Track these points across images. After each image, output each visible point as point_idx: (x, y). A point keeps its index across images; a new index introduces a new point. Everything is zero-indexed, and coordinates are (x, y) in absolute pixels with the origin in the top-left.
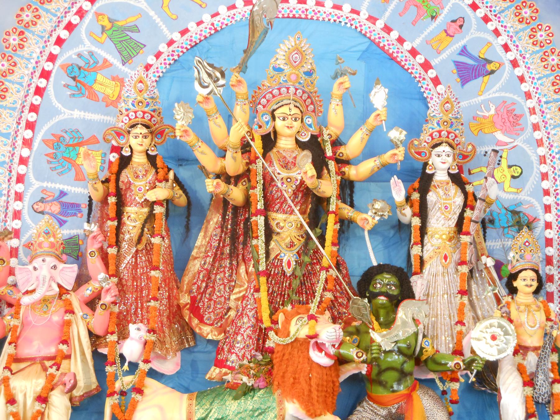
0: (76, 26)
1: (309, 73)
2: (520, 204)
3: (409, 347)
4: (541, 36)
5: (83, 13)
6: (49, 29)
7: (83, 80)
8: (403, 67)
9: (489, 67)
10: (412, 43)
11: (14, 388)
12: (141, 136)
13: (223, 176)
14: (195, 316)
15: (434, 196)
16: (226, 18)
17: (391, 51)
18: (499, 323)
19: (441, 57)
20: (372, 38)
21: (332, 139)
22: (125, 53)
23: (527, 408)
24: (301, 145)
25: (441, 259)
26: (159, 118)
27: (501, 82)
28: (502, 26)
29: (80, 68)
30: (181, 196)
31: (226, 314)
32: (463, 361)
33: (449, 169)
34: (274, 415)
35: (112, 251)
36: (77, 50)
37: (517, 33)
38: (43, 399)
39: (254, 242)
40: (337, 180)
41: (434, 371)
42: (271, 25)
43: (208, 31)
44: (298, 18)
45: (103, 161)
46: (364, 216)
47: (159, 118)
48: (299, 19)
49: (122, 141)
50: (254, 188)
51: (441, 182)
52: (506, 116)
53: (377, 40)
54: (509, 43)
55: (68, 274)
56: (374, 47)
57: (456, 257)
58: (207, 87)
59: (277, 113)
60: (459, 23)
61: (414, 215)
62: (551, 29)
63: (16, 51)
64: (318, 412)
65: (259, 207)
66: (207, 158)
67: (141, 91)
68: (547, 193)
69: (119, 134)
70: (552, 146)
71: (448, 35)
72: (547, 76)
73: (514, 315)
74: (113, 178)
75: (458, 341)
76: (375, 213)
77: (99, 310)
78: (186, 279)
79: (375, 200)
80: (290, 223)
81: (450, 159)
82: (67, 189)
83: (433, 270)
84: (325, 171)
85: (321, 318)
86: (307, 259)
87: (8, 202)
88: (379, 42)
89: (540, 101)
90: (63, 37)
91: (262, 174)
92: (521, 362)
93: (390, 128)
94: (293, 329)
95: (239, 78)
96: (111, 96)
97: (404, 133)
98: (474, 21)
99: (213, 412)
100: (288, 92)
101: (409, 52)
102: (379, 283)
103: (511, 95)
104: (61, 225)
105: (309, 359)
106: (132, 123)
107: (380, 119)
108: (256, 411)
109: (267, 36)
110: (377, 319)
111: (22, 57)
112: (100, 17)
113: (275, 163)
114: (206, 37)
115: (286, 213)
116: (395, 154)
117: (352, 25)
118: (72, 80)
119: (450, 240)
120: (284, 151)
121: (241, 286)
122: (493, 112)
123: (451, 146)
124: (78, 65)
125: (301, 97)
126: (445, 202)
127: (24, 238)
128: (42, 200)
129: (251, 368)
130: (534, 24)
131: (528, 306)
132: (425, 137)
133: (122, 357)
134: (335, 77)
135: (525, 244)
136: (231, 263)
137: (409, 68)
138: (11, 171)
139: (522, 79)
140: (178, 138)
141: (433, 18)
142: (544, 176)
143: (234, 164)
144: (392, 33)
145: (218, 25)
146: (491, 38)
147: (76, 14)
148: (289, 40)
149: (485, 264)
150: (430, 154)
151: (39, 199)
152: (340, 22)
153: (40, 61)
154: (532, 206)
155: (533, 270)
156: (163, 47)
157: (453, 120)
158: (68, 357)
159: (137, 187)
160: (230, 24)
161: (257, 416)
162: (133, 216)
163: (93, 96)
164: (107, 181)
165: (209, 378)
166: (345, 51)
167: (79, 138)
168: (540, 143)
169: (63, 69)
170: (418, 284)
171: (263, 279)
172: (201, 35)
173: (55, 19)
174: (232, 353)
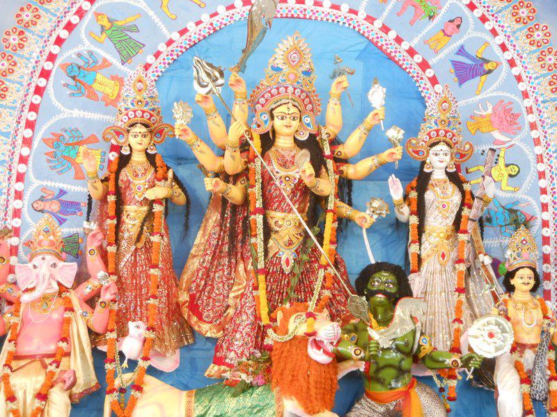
0: (75, 25)
12: (140, 135)
15: (432, 194)
17: (389, 51)
22: (124, 53)
24: (299, 144)
25: (438, 258)
26: (158, 118)
29: (79, 67)
33: (446, 167)
36: (76, 50)
39: (253, 240)
43: (207, 30)
46: (362, 214)
47: (158, 118)
49: (121, 140)
50: (253, 186)
58: (206, 86)
59: (275, 112)
60: (456, 23)
61: (412, 213)
65: (257, 206)
66: (206, 157)
67: (140, 91)
69: (118, 133)
71: (445, 34)
76: (373, 212)
80: (289, 221)
81: (448, 158)
84: (324, 170)
95: (238, 77)
96: (111, 95)
98: (471, 21)
100: (286, 92)
112: (100, 17)
114: (205, 37)
116: (393, 153)
117: (350, 25)
119: (448, 238)
123: (448, 145)
124: (77, 65)
125: (300, 96)
132: (423, 136)
134: (334, 77)
140: (177, 137)
143: (232, 163)
148: (287, 40)
150: (428, 153)
152: (338, 22)
156: (162, 47)
162: (132, 215)
163: (92, 95)
164: (106, 180)
172: (199, 35)
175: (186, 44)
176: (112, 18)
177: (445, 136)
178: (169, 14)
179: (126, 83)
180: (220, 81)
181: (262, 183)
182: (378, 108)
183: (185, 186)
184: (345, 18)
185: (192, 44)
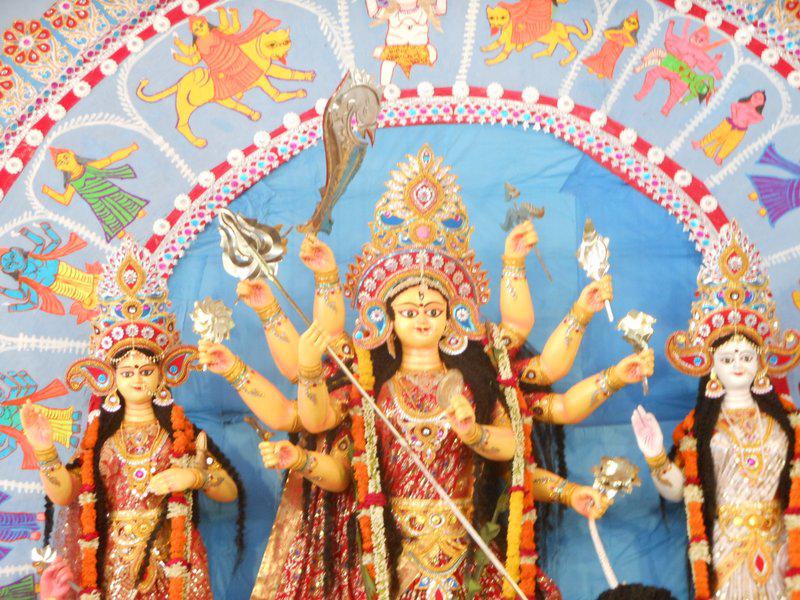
0: (16, 176)
1: (454, 223)
5: (28, 153)
7: (32, 277)
8: (650, 196)
10: (664, 149)
12: (136, 371)
15: (725, 441)
16: (300, 136)
17: (624, 169)
20: (585, 147)
21: (512, 346)
22: (110, 219)
24: (448, 361)
25: (750, 567)
26: (171, 335)
29: (26, 255)
30: (221, 480)
33: (752, 385)
36: (19, 222)
39: (366, 559)
42: (371, 138)
43: (266, 162)
44: (438, 123)
45: (75, 428)
46: (584, 491)
47: (171, 335)
48: (439, 126)
49: (102, 384)
50: (359, 453)
51: (738, 413)
53: (595, 151)
56: (591, 164)
58: (247, 264)
59: (396, 305)
60: (754, 103)
61: (688, 481)
62: (4, 47)
65: (371, 490)
66: (261, 399)
67: (131, 286)
69: (96, 372)
71: (734, 127)
76: (607, 484)
79: (606, 458)
80: (435, 517)
81: (752, 366)
82: (9, 488)
84: (501, 409)
88: (600, 154)
91: (373, 424)
95: (318, 243)
96: (87, 302)
97: (650, 320)
98: (784, 95)
100: (414, 262)
107: (598, 300)
112: (61, 157)
113: (397, 400)
114: (263, 176)
115: (427, 497)
116: (635, 365)
117: (542, 126)
118: (10, 278)
119: (766, 527)
120: (415, 376)
123: (751, 339)
124: (21, 250)
125: (442, 269)
132: (697, 326)
134: (508, 226)
137: (661, 199)
140: (205, 368)
141: (702, 97)
143: (315, 409)
145: (284, 151)
147: (14, 155)
148: (408, 163)
150: (712, 360)
152: (520, 123)
156: (182, 202)
157: (749, 289)
159: (134, 469)
160: (307, 147)
162: (128, 528)
163: (52, 305)
164: (76, 465)
166: (535, 176)
167: (29, 387)
172: (253, 172)
175: (227, 192)
176: (85, 154)
177: (742, 322)
178: (191, 138)
179: (103, 279)
180: (275, 251)
181: (379, 445)
182: (596, 276)
183: (233, 463)
184: (533, 113)
185: (240, 190)
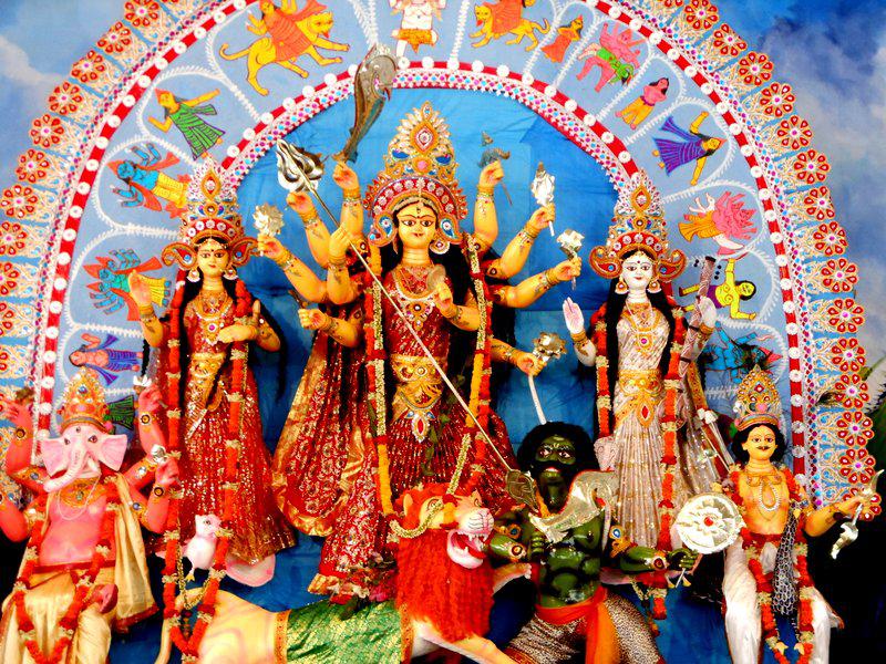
0: (129, 109)
1: (445, 159)
2: (754, 335)
3: (590, 539)
4: (777, 100)
6: (93, 115)
7: (139, 183)
9: (705, 146)
11: (31, 608)
12: (212, 254)
13: (327, 306)
14: (294, 505)
15: (627, 326)
16: (336, 91)
17: (566, 128)
18: (715, 500)
19: (636, 135)
20: (540, 111)
22: (196, 144)
23: (763, 624)
27: (722, 166)
28: (722, 88)
29: (135, 166)
30: (269, 335)
31: (336, 500)
32: (667, 557)
33: (648, 287)
34: (397, 639)
35: (173, 414)
36: (131, 142)
37: (742, 98)
38: (70, 622)
40: (487, 308)
41: (631, 573)
43: (311, 109)
44: (435, 87)
46: (528, 355)
49: (188, 262)
50: (369, 320)
51: (637, 306)
52: (731, 214)
53: (547, 114)
54: (732, 111)
55: (113, 448)
56: (543, 123)
57: (659, 410)
59: (401, 216)
63: (48, 145)
64: (459, 633)
65: (376, 347)
66: (301, 279)
67: (211, 192)
68: (791, 318)
69: (183, 253)
70: (796, 252)
72: (786, 156)
73: (744, 490)
74: (175, 313)
75: (663, 529)
77: (153, 496)
78: (281, 452)
79: (543, 334)
80: (421, 369)
81: (648, 274)
83: (628, 431)
85: (464, 501)
86: (445, 418)
87: (36, 353)
89: (778, 191)
90: (111, 124)
92: (755, 557)
93: (558, 233)
94: (423, 517)
95: (346, 168)
97: (580, 237)
99: (311, 636)
100: (415, 186)
101: (592, 128)
102: (548, 450)
103: (737, 184)
104: (109, 382)
105: (448, 561)
106: (200, 236)
108: (371, 634)
109: (384, 110)
110: (547, 502)
111: (58, 155)
112: (163, 96)
113: (398, 284)
114: (308, 119)
117: (510, 94)
121: (356, 460)
122: (712, 207)
123: (649, 254)
124: (132, 163)
126: (642, 335)
127: (59, 401)
128: (83, 349)
129: (367, 574)
130: (766, 85)
131: (763, 477)
133: (187, 563)
134: (483, 165)
135: (756, 389)
136: (342, 428)
137: (592, 151)
138: (40, 310)
139: (752, 161)
140: (262, 254)
142: (787, 295)
143: (339, 287)
144: (567, 104)
145: (324, 101)
146: (707, 105)
149: (704, 420)
151: (78, 347)
152: (494, 91)
153: (80, 159)
154: (770, 337)
155: (768, 425)
156: (249, 134)
158: (111, 564)
160: (341, 99)
161: (374, 641)
162: (202, 365)
165: (312, 590)
166: (504, 130)
168: (780, 249)
169: (111, 167)
170: (606, 450)
171: (382, 448)
172: (301, 115)
173: (101, 100)
174: (343, 554)
